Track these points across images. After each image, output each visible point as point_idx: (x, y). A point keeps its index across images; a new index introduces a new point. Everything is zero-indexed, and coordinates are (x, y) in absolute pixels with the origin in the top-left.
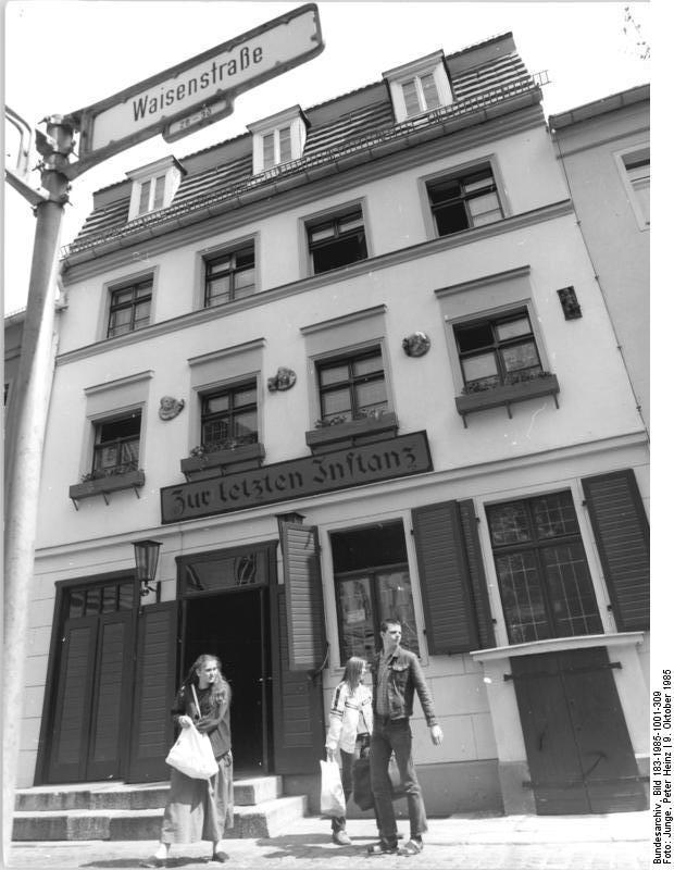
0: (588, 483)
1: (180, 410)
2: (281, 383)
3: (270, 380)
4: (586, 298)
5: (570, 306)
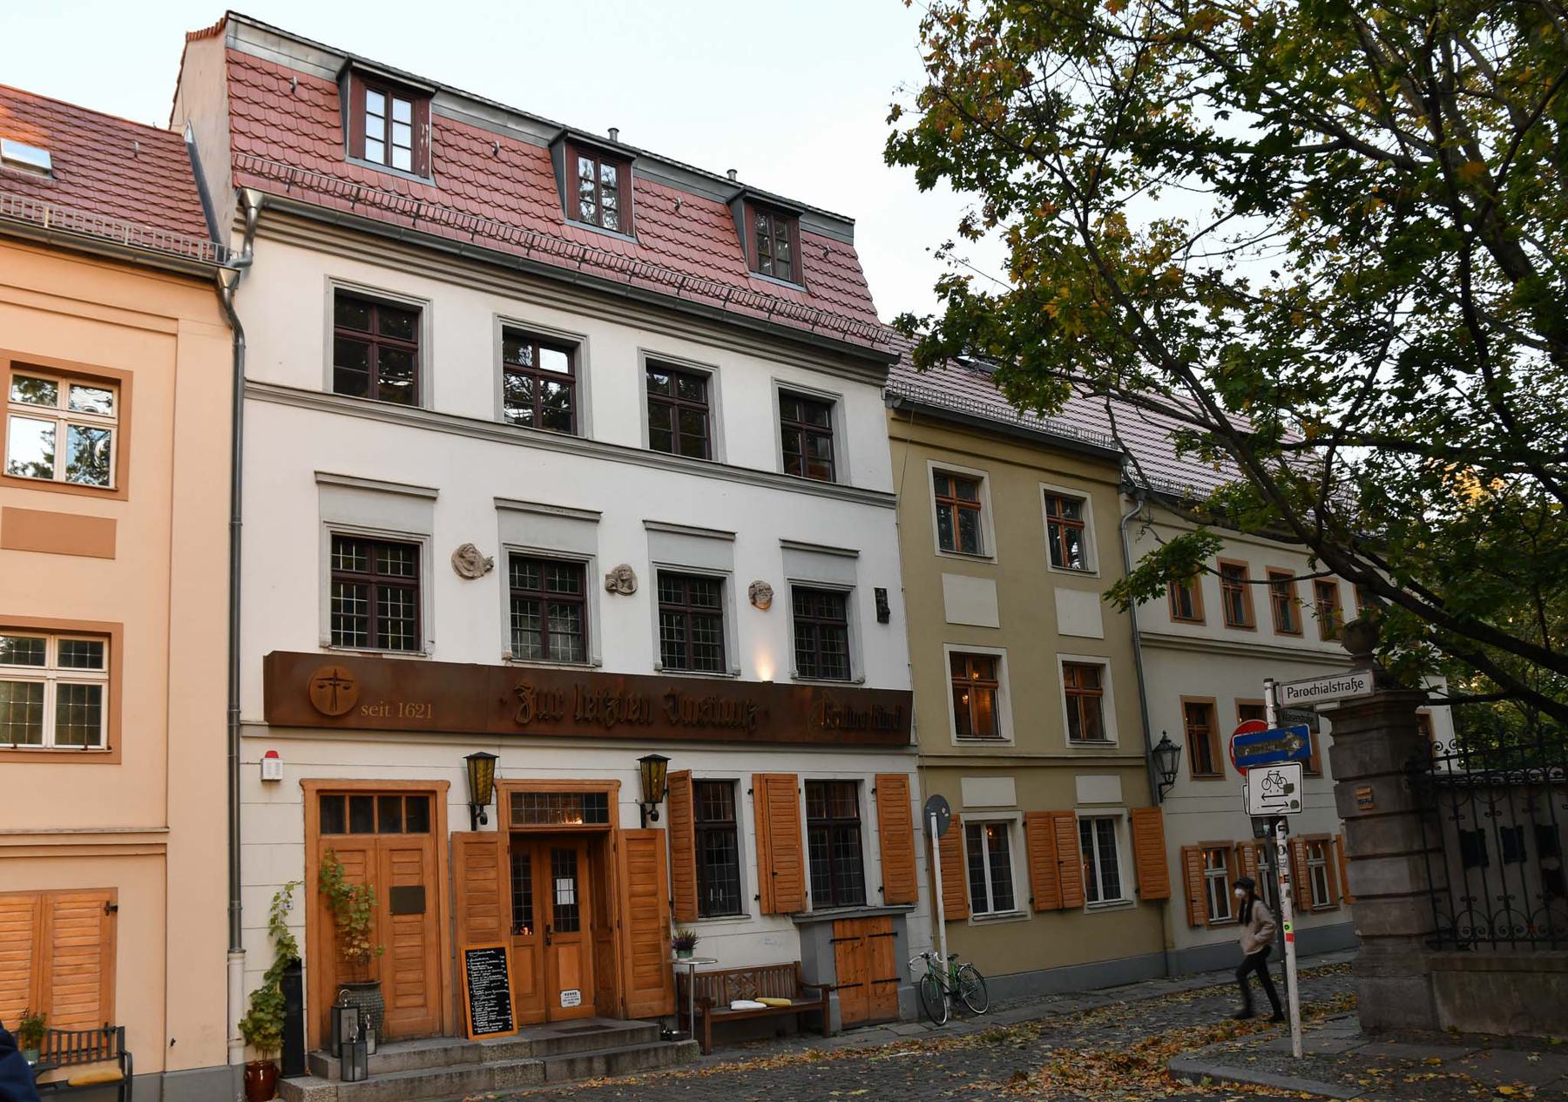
0: (879, 778)
1: (488, 570)
2: (621, 583)
3: (608, 577)
4: (895, 603)
5: (883, 615)
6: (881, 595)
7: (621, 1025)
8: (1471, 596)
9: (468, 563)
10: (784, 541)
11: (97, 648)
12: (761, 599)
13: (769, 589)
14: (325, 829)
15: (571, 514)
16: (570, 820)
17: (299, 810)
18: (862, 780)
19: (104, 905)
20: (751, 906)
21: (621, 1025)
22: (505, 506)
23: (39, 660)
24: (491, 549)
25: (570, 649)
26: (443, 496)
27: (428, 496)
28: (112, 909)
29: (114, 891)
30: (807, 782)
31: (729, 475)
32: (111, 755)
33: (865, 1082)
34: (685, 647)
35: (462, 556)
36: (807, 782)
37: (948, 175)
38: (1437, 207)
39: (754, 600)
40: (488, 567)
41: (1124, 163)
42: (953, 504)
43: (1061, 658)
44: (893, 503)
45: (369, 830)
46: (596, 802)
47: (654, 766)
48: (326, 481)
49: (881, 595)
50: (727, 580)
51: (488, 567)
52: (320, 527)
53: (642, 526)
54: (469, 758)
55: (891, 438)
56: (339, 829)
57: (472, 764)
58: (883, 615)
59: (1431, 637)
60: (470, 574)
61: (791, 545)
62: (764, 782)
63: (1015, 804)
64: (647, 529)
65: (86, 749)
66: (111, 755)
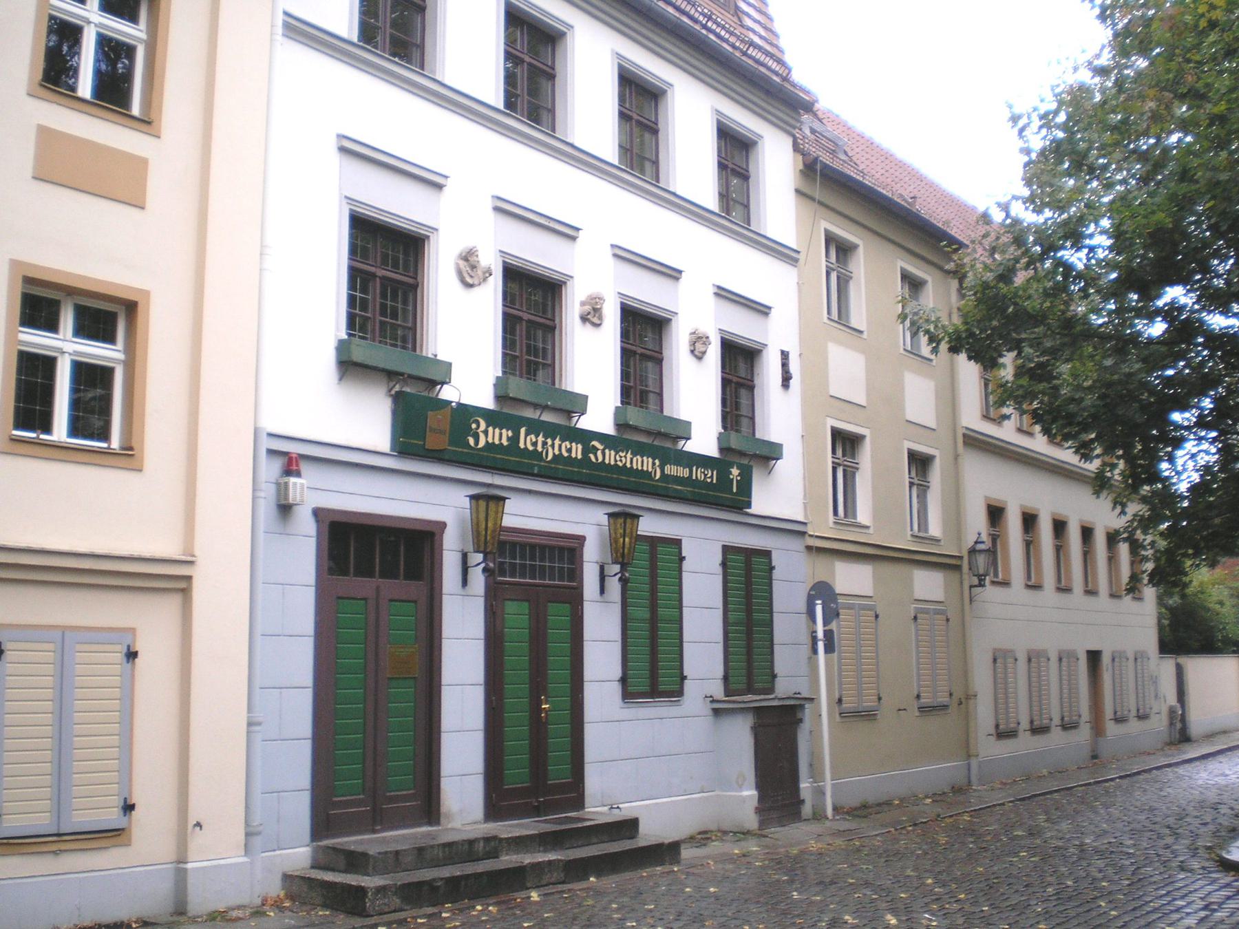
2: (592, 316)
6: (785, 355)
10: (719, 287)
11: (110, 319)
13: (707, 338)
14: (331, 571)
15: (552, 225)
17: (312, 543)
18: (909, 449)
19: (125, 650)
22: (505, 210)
23: (52, 325)
24: (490, 259)
28: (132, 655)
31: (679, 207)
33: (1200, 348)
34: (632, 390)
35: (466, 259)
37: (1046, 436)
38: (1082, 451)
39: (597, 311)
42: (834, 270)
43: (908, 445)
44: (796, 260)
45: (370, 574)
47: (629, 521)
48: (352, 150)
49: (785, 355)
50: (673, 322)
51: (489, 273)
52: (340, 201)
53: (609, 252)
54: (472, 497)
55: (798, 191)
56: (344, 572)
57: (612, 521)
58: (786, 379)
59: (572, 908)
60: (469, 280)
61: (742, 300)
63: (870, 594)
64: (615, 255)
65: (38, 438)
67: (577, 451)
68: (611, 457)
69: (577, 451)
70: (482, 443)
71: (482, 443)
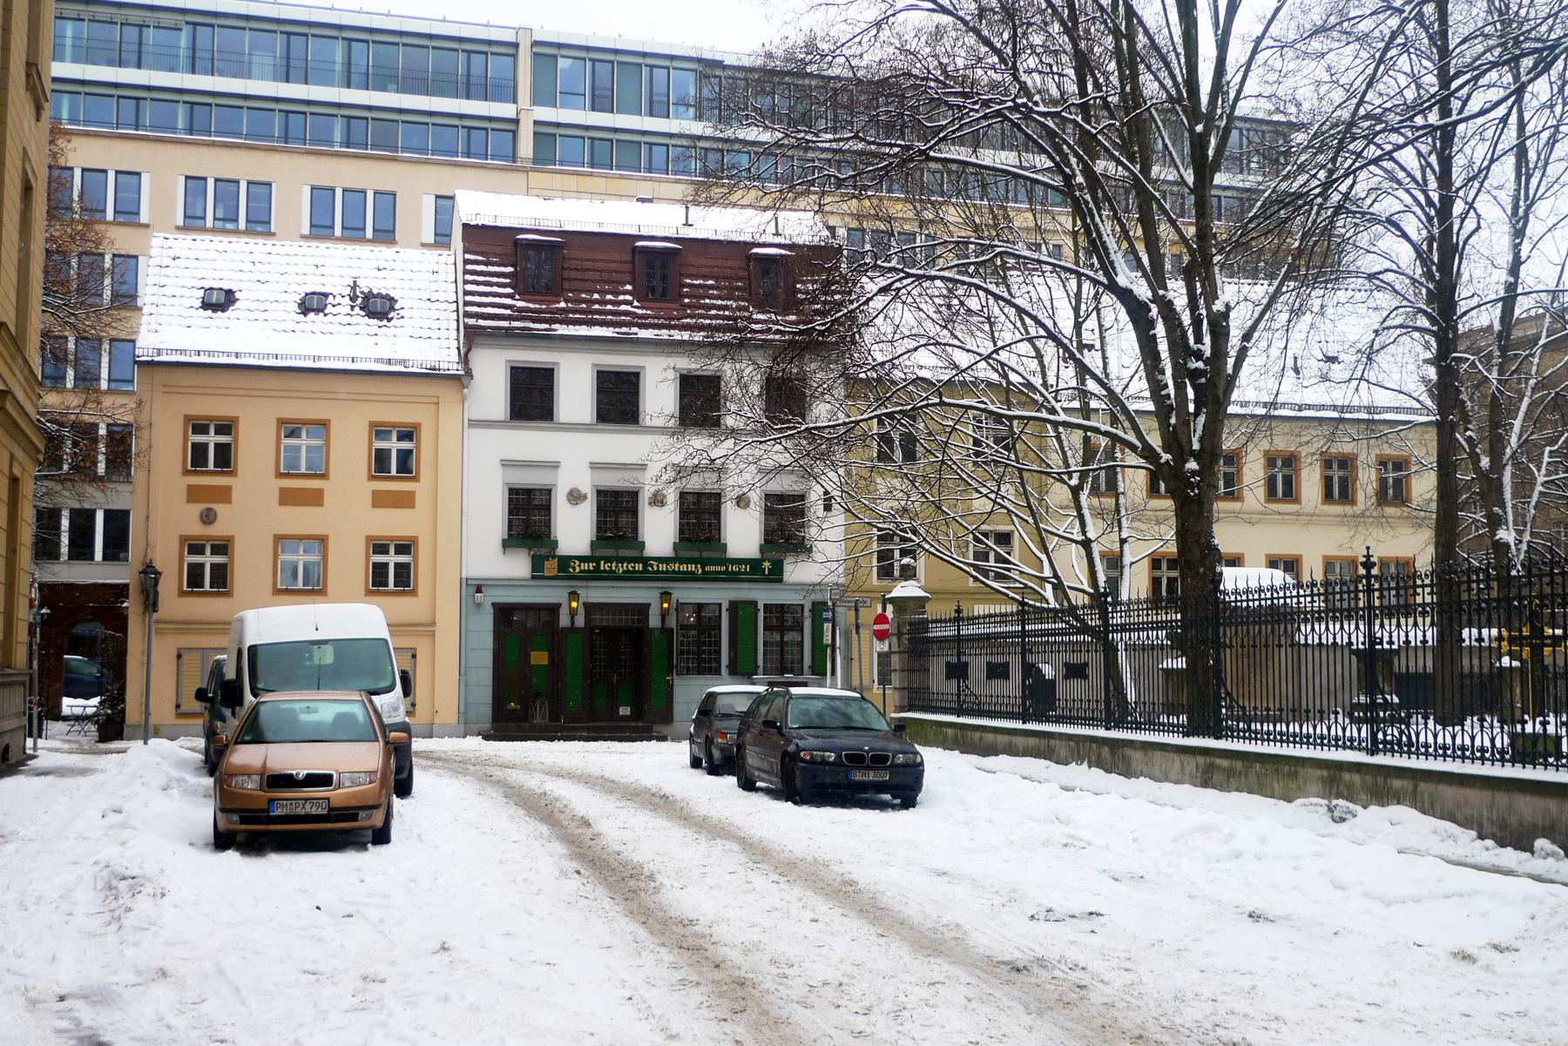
2: (658, 500)
7: (11, 671)
8: (1508, 456)
9: (575, 497)
12: (742, 504)
16: (1166, 386)
20: (724, 671)
21: (11, 671)
22: (594, 466)
24: (587, 488)
25: (1106, 114)
26: (563, 465)
27: (554, 466)
28: (414, 656)
29: (415, 649)
30: (766, 606)
32: (414, 593)
36: (766, 606)
40: (585, 497)
41: (136, 944)
46: (643, 609)
51: (585, 497)
62: (734, 606)
66: (414, 593)
67: (639, 567)
68: (663, 567)
69: (639, 567)
70: (578, 570)
71: (578, 570)
